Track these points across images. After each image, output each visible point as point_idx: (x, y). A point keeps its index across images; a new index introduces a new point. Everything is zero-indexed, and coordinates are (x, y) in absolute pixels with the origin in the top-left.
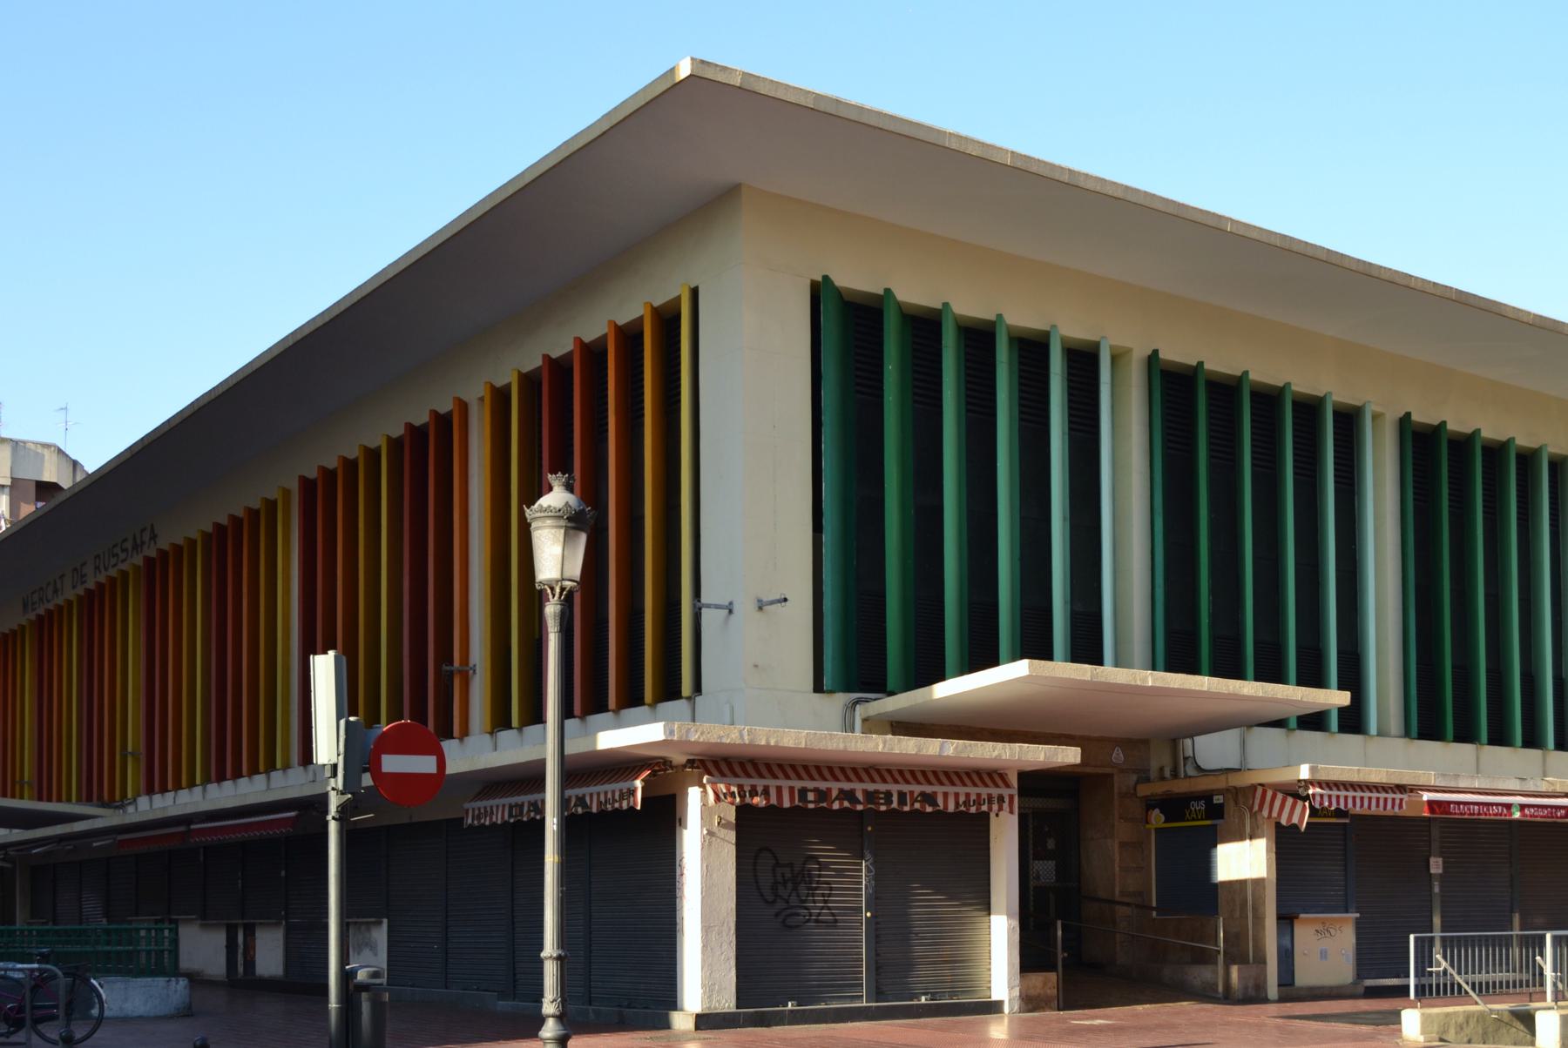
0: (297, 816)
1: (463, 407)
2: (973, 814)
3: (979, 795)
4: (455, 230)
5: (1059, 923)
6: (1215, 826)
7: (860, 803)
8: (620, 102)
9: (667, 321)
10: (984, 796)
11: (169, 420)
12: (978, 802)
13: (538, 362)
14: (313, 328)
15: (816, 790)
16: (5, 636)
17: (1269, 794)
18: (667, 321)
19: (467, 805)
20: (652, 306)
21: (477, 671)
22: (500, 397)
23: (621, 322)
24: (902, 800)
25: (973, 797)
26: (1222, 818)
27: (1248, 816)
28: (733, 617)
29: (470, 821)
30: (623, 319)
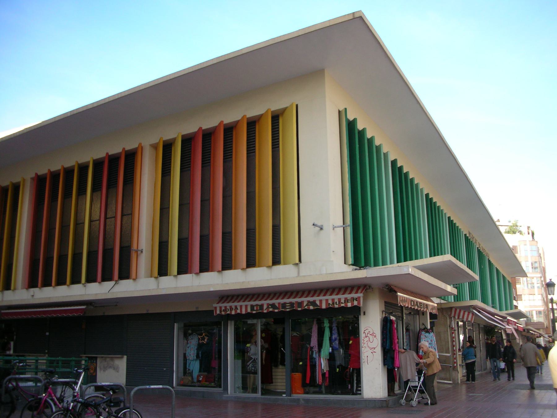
0: (85, 308)
1: (24, 180)
2: (243, 314)
3: (226, 307)
4: (194, 69)
5: (341, 354)
6: (434, 322)
7: (255, 310)
8: (137, 86)
9: (276, 118)
10: (228, 308)
11: (170, 75)
12: (225, 310)
13: (104, 155)
14: (103, 102)
15: (257, 305)
16: (5, 190)
17: (458, 310)
18: (276, 118)
19: (215, 305)
20: (78, 162)
21: (144, 252)
22: (168, 147)
23: (52, 170)
24: (252, 309)
25: (223, 308)
26: (437, 319)
27: (448, 318)
28: (322, 231)
29: (218, 312)
30: (128, 148)
